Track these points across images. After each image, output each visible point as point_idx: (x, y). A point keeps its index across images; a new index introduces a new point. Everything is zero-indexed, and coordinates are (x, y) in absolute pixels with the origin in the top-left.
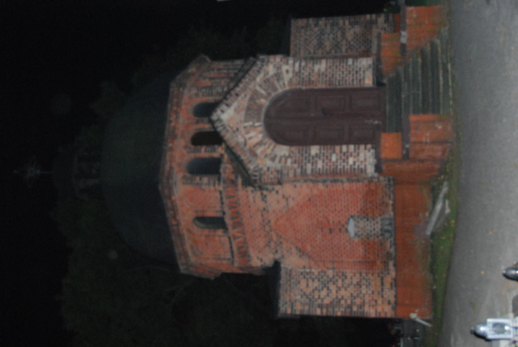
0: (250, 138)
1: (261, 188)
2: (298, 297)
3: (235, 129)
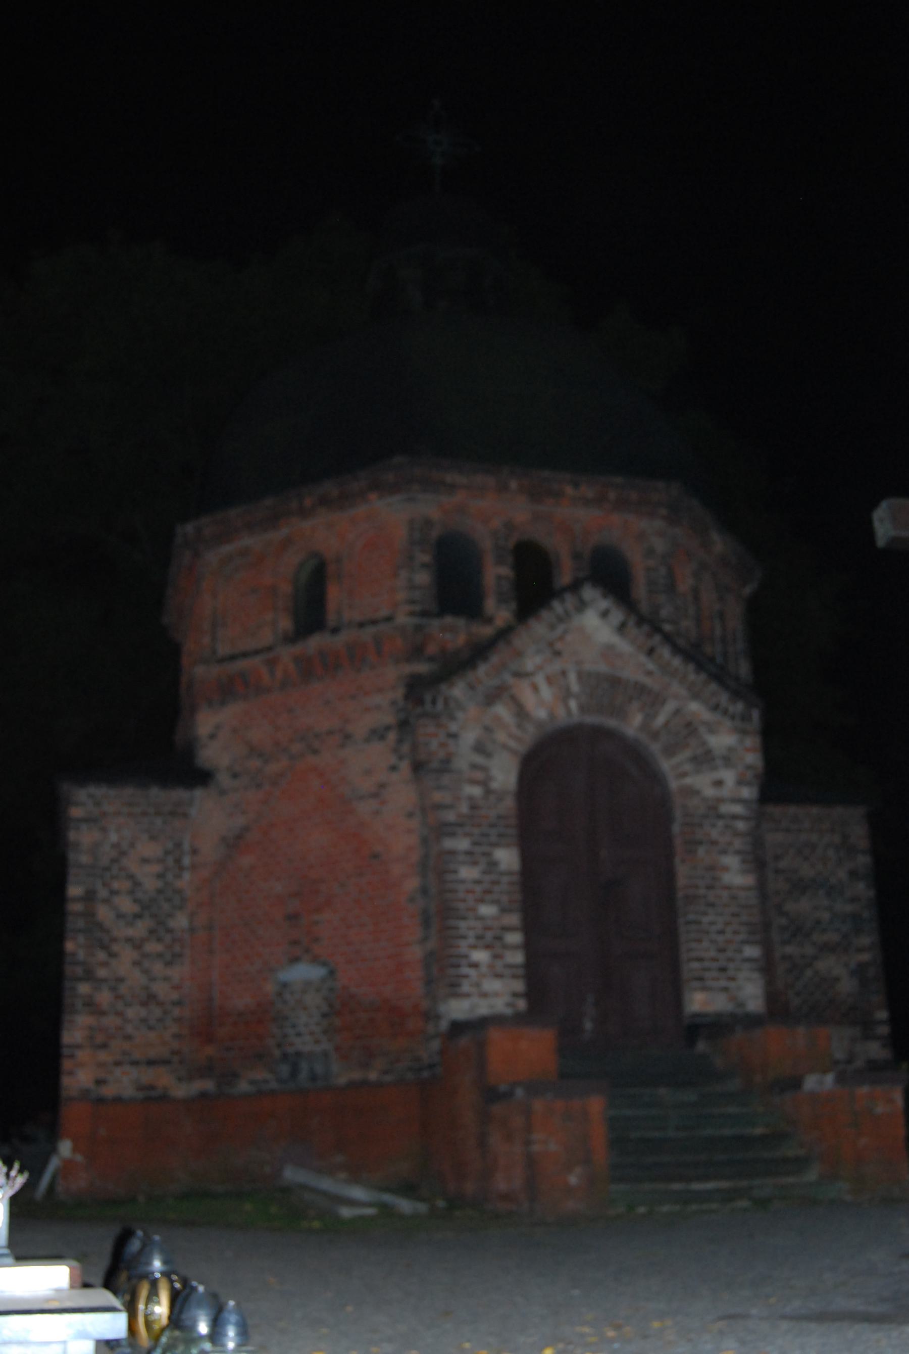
0: (535, 688)
1: (404, 725)
2: (114, 837)
3: (559, 646)
